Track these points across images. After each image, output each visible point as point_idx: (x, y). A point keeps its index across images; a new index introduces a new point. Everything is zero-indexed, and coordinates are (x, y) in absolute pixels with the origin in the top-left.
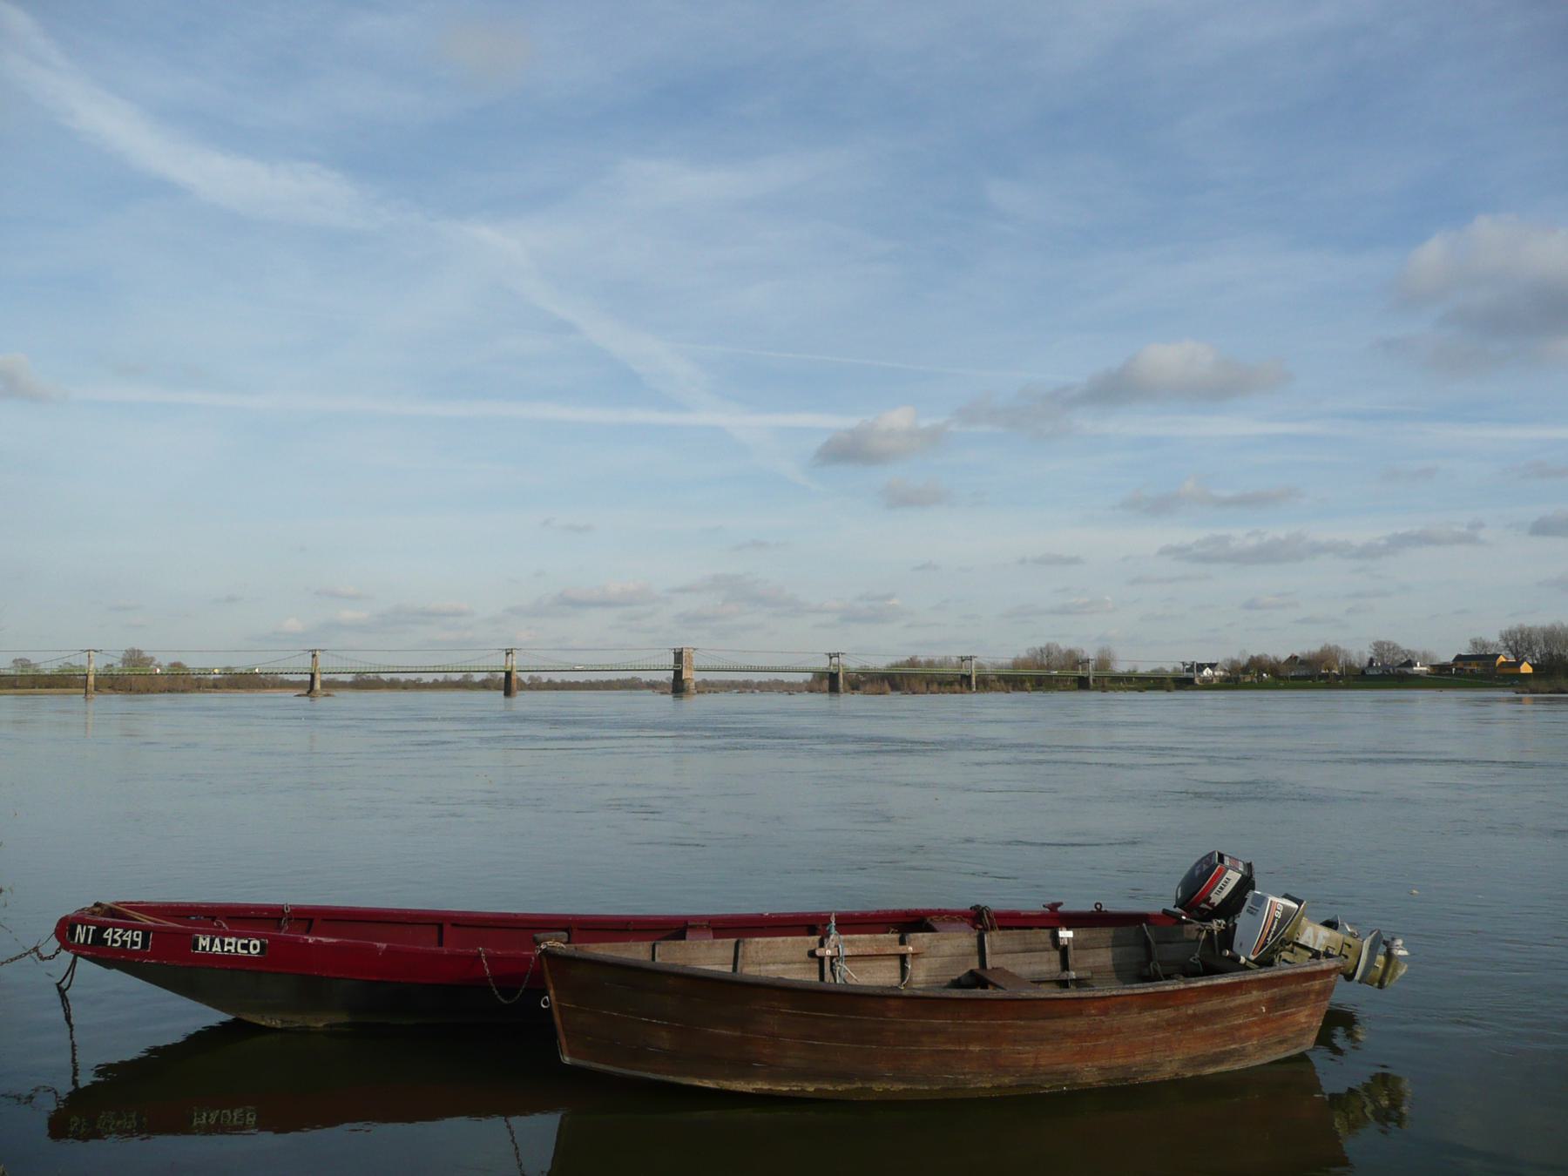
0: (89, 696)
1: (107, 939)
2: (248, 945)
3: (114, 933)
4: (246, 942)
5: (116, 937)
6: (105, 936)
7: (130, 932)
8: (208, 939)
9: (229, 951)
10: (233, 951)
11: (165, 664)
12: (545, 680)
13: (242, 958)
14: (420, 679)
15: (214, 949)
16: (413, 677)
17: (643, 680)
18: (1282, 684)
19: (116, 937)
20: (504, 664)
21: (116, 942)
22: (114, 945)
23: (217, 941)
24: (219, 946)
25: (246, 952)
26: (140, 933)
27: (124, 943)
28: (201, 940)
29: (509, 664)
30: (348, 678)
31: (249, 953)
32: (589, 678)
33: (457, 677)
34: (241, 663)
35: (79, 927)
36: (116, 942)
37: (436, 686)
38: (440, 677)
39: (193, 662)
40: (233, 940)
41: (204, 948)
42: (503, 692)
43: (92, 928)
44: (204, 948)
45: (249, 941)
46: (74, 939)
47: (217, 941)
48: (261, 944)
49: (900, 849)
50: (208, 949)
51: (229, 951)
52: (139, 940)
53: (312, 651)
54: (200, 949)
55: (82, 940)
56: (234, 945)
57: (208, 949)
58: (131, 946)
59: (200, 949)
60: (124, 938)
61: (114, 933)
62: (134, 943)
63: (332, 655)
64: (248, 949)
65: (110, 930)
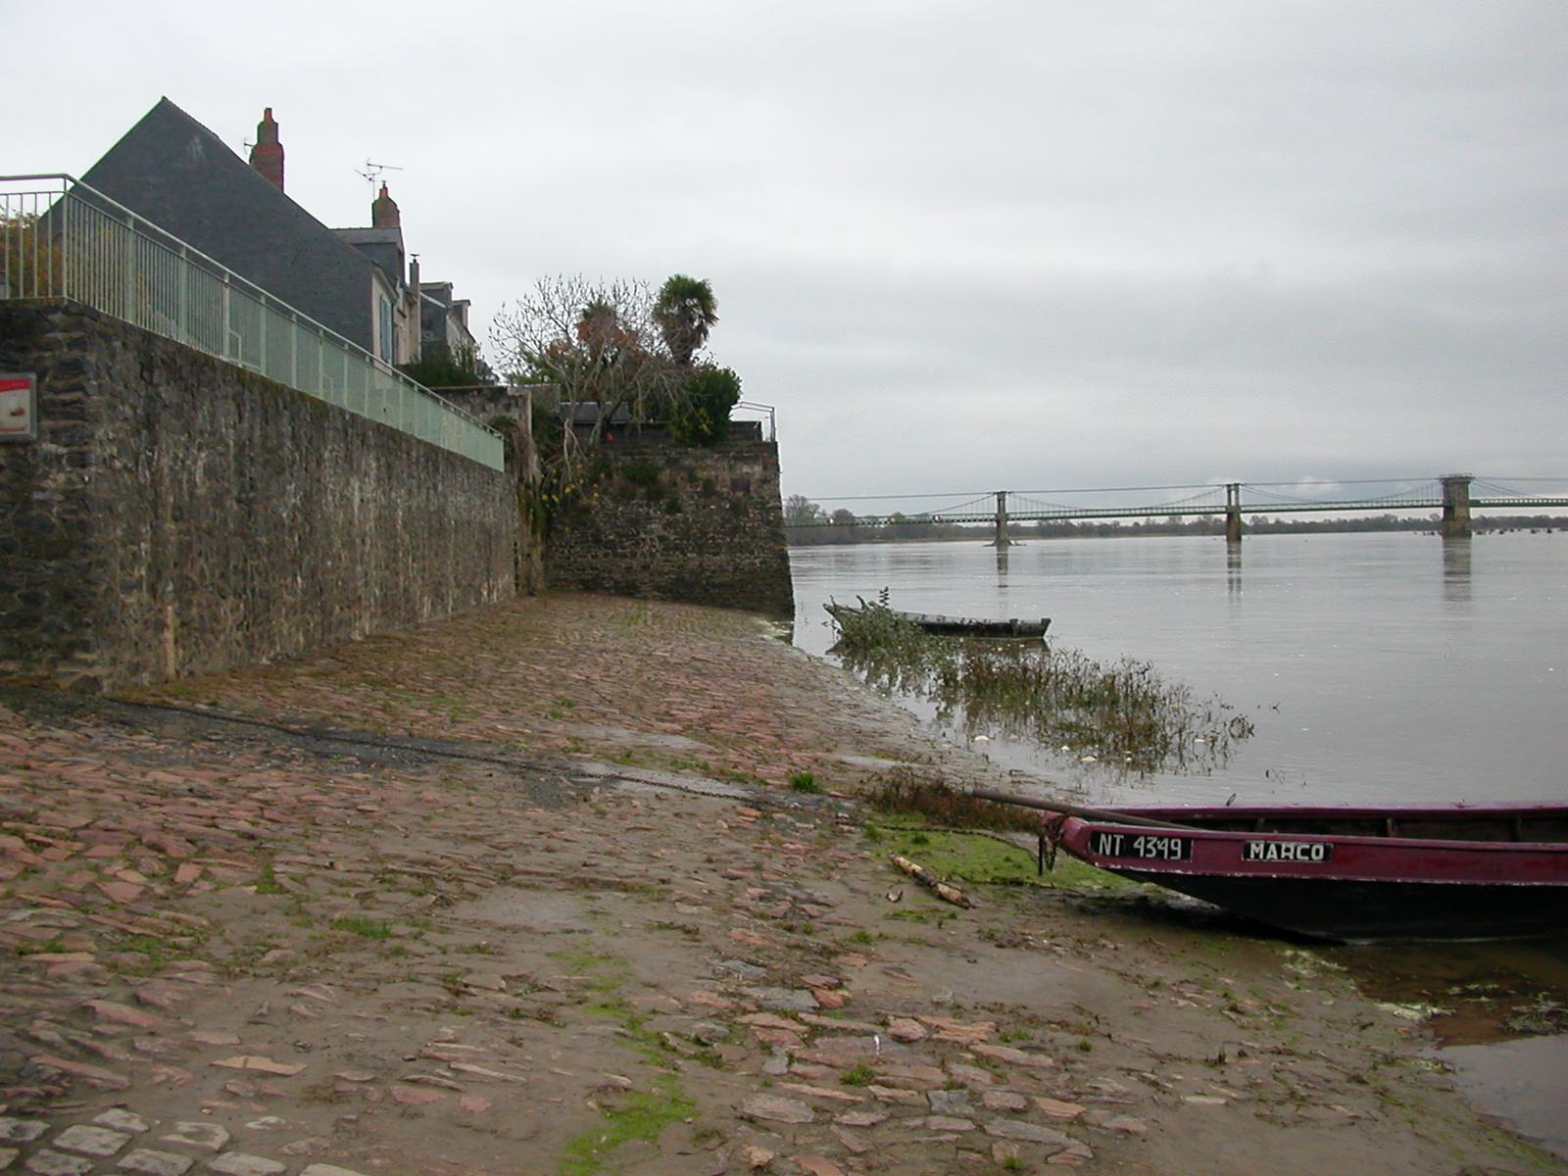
0: (1011, 579)
1: (1139, 850)
2: (1309, 851)
3: (1147, 842)
4: (1308, 847)
5: (1149, 846)
6: (1136, 845)
7: (1166, 841)
8: (1262, 846)
9: (1287, 858)
10: (1291, 857)
11: (830, 513)
12: (1272, 521)
13: (1304, 865)
14: (1117, 523)
15: (1268, 857)
16: (1109, 521)
17: (479, 356)
18: (1269, 975)
19: (1149, 846)
20: (1226, 504)
21: (1150, 852)
22: (1148, 856)
23: (1273, 847)
24: (1275, 852)
25: (1307, 858)
26: (1179, 842)
27: (1160, 853)
28: (1253, 846)
29: (1233, 504)
30: (1033, 524)
31: (1311, 859)
32: (1328, 518)
33: (1162, 520)
34: (910, 510)
35: (1103, 837)
36: (1150, 852)
37: (1136, 531)
38: (1142, 521)
39: (859, 511)
40: (1292, 846)
41: (1257, 856)
42: (1225, 537)
43: (1118, 838)
44: (1257, 856)
45: (1311, 846)
46: (1098, 851)
47: (1273, 847)
48: (1325, 848)
49: (1416, 1134)
50: (1261, 856)
51: (1287, 858)
52: (1179, 849)
53: (998, 493)
54: (1252, 856)
55: (1108, 852)
56: (1292, 850)
57: (1261, 856)
58: (1169, 856)
59: (1252, 856)
60: (1160, 847)
61: (1147, 842)
62: (1172, 853)
63: (1020, 498)
64: (1310, 855)
65: (1142, 839)
